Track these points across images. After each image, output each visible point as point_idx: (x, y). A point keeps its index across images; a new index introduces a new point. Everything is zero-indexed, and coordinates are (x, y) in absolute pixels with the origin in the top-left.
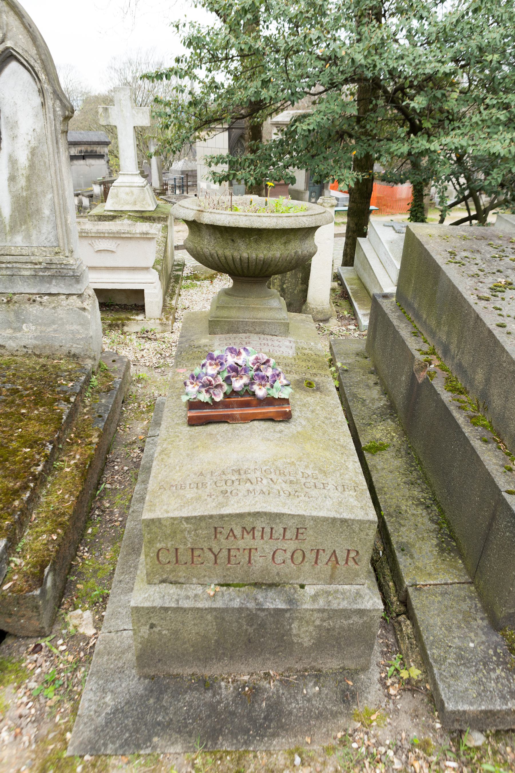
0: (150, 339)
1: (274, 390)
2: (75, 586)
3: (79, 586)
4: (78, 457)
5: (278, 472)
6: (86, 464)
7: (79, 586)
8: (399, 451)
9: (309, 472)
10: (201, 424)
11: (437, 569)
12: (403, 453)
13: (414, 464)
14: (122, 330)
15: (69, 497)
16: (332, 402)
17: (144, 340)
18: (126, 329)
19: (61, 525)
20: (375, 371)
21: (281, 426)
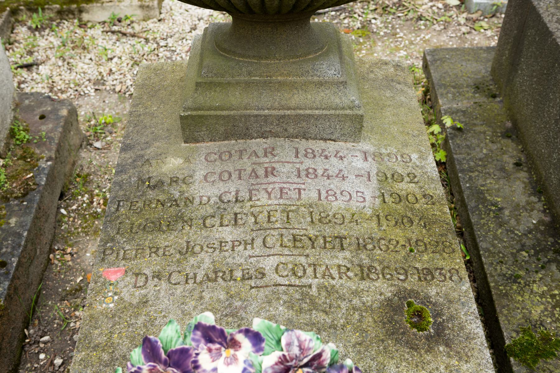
0: (124, 34)
14: (80, 20)
17: (115, 37)
18: (85, 17)
20: (514, 133)
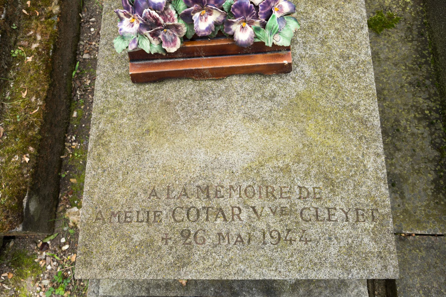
1: (267, 32)
2: (69, 181)
3: (72, 180)
4: (39, 38)
5: (264, 192)
6: (48, 49)
7: (72, 180)
8: (409, 29)
9: (310, 185)
10: (154, 82)
11: (427, 216)
12: (415, 33)
13: (425, 52)
15: (36, 100)
16: (354, 15)
19: (31, 141)
21: (273, 84)
